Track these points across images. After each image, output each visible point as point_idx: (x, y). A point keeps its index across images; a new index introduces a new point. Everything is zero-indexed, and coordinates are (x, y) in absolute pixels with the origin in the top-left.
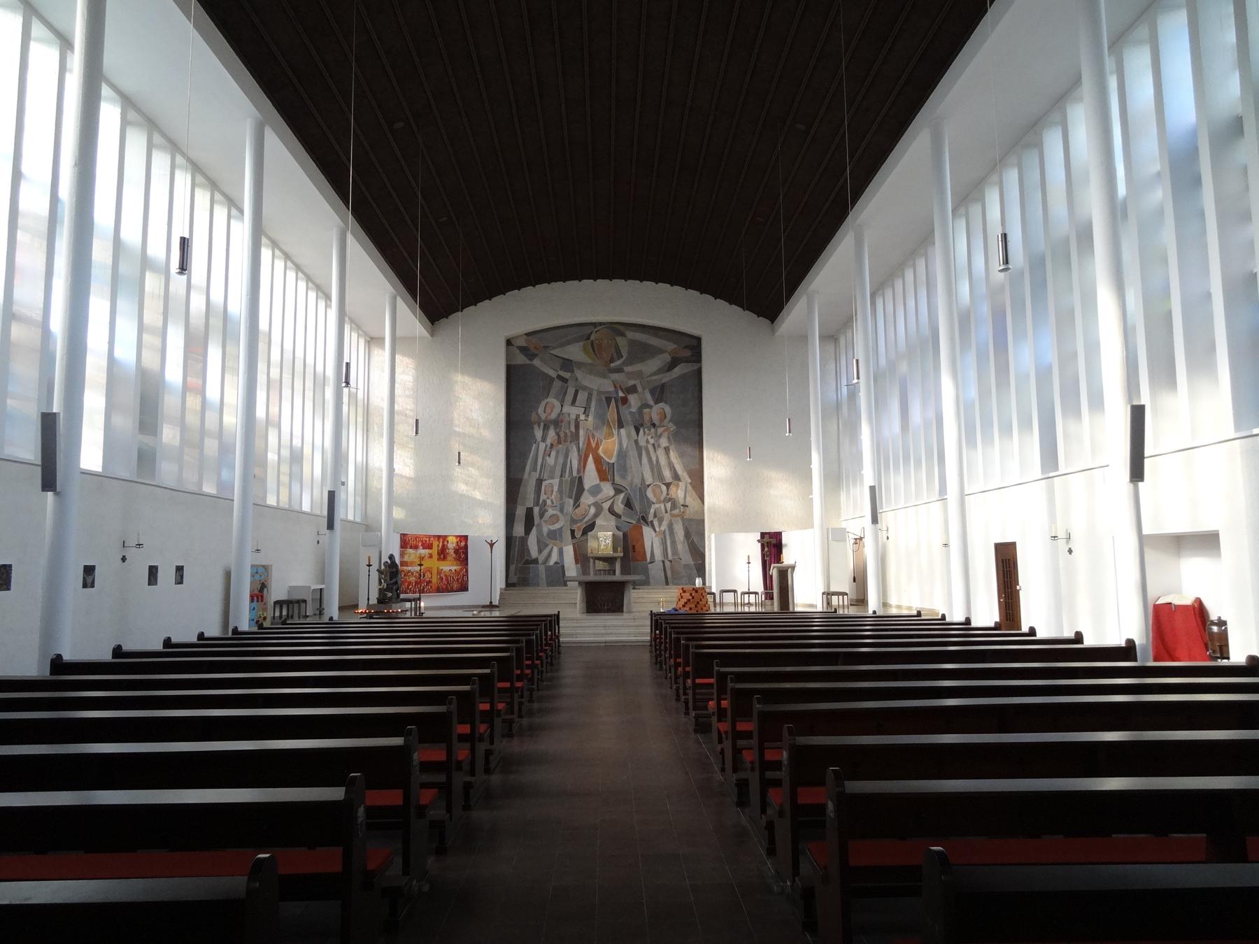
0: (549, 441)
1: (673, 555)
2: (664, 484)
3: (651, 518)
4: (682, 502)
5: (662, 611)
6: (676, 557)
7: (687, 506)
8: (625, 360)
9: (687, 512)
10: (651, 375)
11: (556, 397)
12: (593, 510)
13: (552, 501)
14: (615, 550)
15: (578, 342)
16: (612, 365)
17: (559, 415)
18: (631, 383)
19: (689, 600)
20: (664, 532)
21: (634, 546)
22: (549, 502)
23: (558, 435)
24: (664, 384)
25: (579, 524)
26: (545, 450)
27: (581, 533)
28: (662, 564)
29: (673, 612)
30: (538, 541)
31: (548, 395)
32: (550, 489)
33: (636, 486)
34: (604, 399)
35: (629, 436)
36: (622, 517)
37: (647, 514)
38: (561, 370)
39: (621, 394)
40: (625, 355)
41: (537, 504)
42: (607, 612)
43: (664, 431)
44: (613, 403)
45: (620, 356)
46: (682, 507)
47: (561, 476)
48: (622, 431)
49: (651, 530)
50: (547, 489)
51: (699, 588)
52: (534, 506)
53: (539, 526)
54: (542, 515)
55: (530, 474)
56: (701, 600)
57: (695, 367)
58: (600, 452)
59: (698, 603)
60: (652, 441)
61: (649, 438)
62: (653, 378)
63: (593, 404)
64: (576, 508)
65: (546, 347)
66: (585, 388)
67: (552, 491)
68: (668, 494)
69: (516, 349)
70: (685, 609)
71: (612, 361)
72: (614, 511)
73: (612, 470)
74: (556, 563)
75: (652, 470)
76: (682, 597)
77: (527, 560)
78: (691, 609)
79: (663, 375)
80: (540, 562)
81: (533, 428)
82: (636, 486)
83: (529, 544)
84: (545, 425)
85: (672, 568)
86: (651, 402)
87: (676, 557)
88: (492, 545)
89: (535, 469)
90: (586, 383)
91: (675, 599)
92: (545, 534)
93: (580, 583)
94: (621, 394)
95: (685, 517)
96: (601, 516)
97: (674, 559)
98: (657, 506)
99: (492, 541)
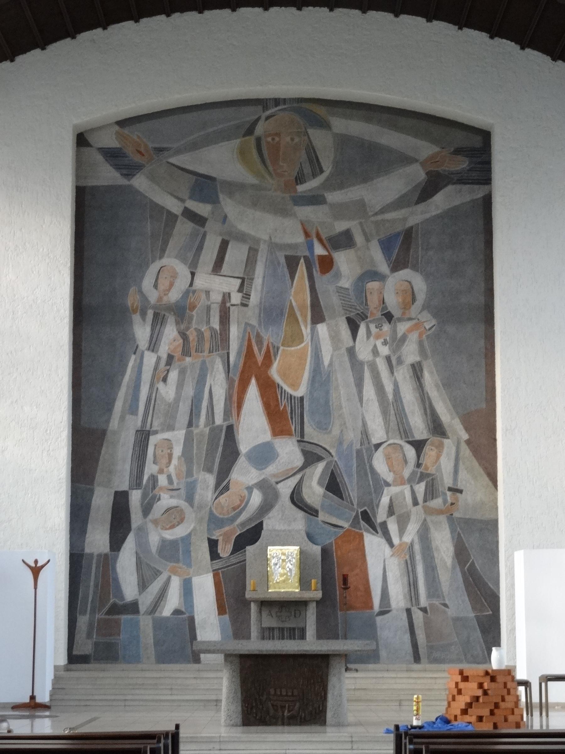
0: (164, 350)
1: (430, 595)
2: (410, 443)
3: (381, 516)
4: (448, 481)
5: (415, 723)
6: (436, 602)
7: (461, 492)
8: (327, 179)
9: (461, 503)
10: (383, 211)
11: (182, 258)
12: (256, 499)
13: (169, 478)
14: (304, 583)
15: (229, 138)
16: (301, 188)
17: (186, 294)
18: (341, 226)
19: (477, 698)
20: (412, 545)
21: (345, 579)
22: (162, 480)
23: (184, 335)
24: (412, 228)
25: (227, 529)
26: (156, 369)
27: (230, 547)
28: (405, 615)
29: (444, 729)
30: (139, 564)
31: (163, 250)
32: (167, 451)
33: (351, 445)
34: (283, 260)
35: (335, 338)
36: (321, 514)
37: (374, 505)
38: (191, 198)
39: (319, 250)
40: (328, 169)
41: (137, 482)
42: (289, 724)
43: (410, 330)
44: (302, 268)
45: (317, 169)
46: (449, 494)
47: (190, 424)
48: (322, 329)
49: (383, 541)
50: (159, 452)
51: (499, 671)
52: (131, 488)
53: (141, 529)
54: (147, 509)
55: (122, 418)
56: (503, 700)
57: (479, 192)
58: (274, 372)
59: (497, 705)
60: (384, 351)
61: (379, 343)
62: (389, 216)
63: (260, 270)
64: (221, 493)
65: (160, 150)
66: (242, 237)
67: (170, 456)
68: (418, 465)
69: (99, 158)
70: (467, 718)
71: (300, 179)
72: (302, 500)
73: (298, 411)
74: (177, 612)
75: (385, 413)
76: (460, 692)
77: (114, 606)
78: (480, 719)
79: (410, 209)
80: (142, 608)
81: (131, 323)
82: (351, 445)
83: (119, 570)
84: (156, 315)
85: (427, 624)
86: (384, 268)
87: (436, 602)
88: (36, 571)
89: (132, 409)
90: (243, 227)
91: (444, 695)
92: (154, 549)
93: (229, 656)
94: (319, 250)
95: (456, 515)
96: (274, 513)
97: (431, 605)
98: (394, 490)
99: (36, 562)
